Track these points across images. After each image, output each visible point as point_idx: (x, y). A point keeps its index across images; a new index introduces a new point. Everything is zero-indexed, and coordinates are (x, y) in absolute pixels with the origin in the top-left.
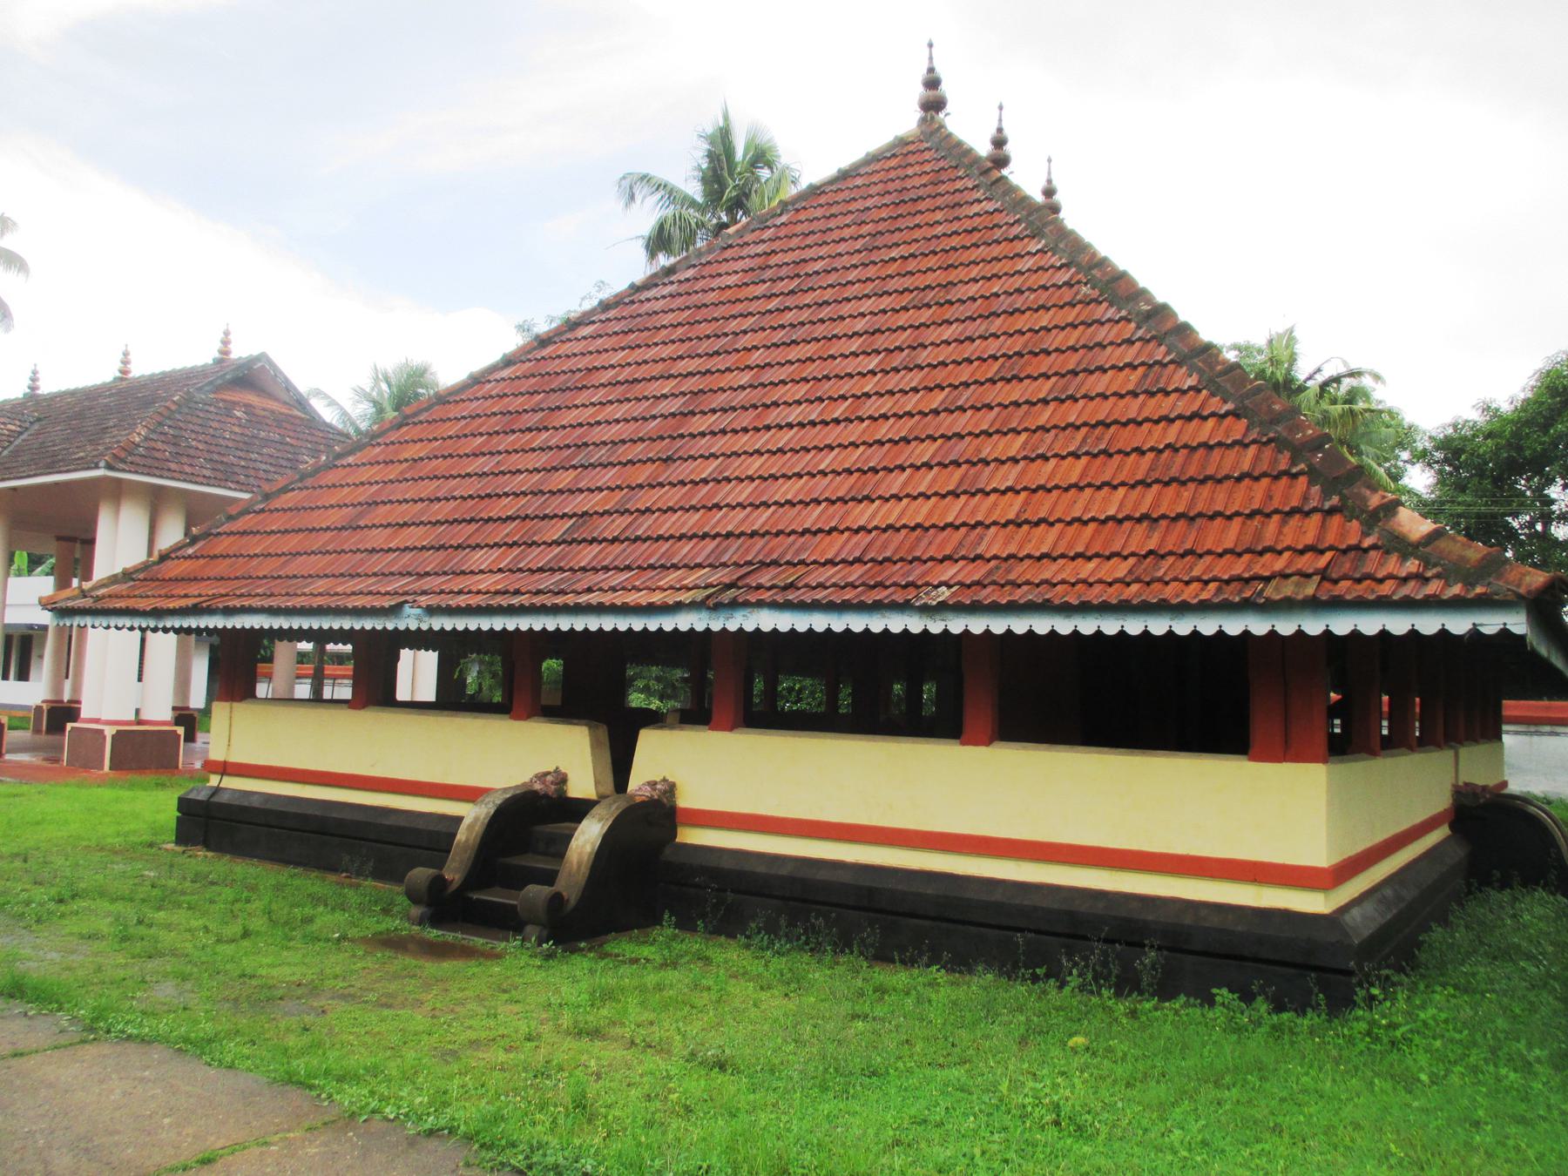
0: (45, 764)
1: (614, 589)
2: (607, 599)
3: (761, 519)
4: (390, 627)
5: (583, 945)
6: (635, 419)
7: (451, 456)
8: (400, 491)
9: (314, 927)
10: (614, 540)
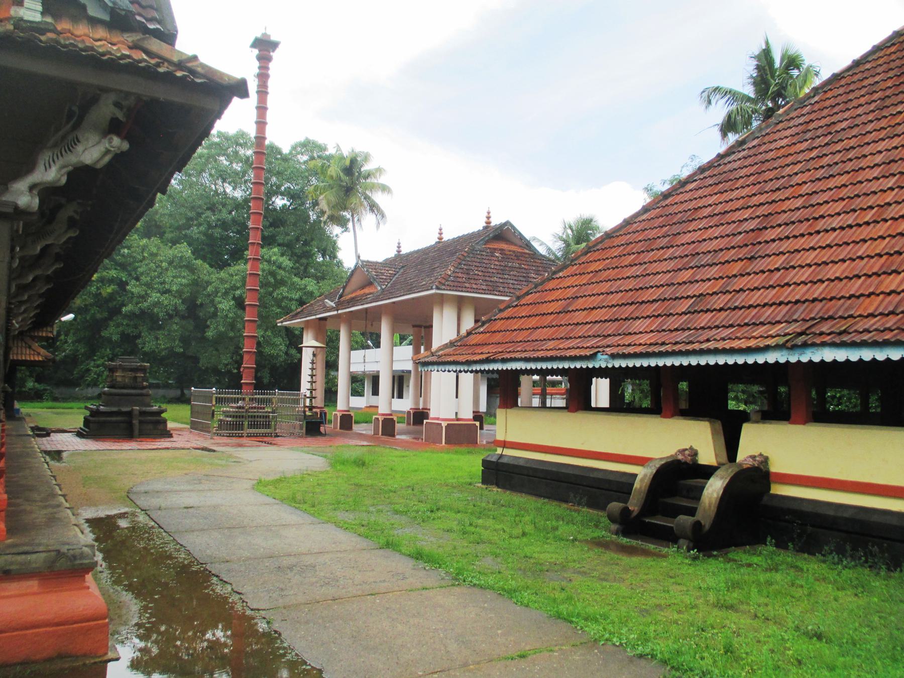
0: (415, 441)
1: (723, 339)
2: (720, 345)
3: (818, 291)
4: (591, 366)
5: (715, 553)
6: (728, 236)
7: (617, 267)
8: (589, 290)
9: (558, 533)
10: (721, 309)
